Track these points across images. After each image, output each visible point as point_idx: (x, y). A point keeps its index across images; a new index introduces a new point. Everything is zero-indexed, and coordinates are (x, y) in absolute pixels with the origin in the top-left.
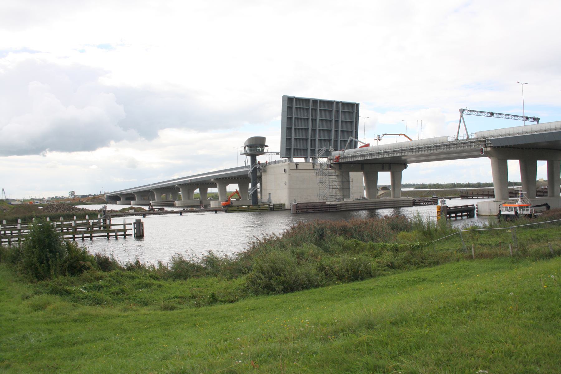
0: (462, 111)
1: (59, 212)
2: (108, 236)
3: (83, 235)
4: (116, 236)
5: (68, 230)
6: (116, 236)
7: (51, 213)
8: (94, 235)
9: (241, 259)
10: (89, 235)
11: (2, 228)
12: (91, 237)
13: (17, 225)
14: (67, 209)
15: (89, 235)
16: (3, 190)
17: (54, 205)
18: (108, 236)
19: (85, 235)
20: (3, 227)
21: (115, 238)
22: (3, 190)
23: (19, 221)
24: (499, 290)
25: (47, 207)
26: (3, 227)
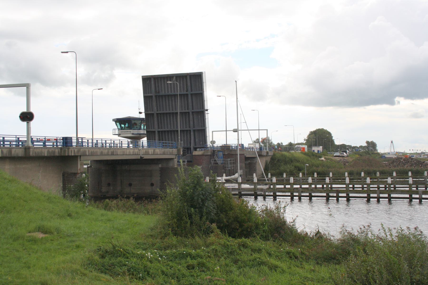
0: (267, 130)
1: (405, 167)
2: (411, 199)
3: (378, 195)
4: (338, 197)
5: (417, 189)
6: (338, 197)
7: (397, 168)
8: (392, 195)
9: (289, 228)
10: (386, 195)
11: (391, 181)
12: (311, 197)
13: (409, 179)
14: (415, 164)
15: (386, 195)
16: (392, 142)
17: (401, 158)
18: (411, 199)
19: (381, 195)
20: (392, 180)
21: (325, 201)
22: (392, 142)
23: (410, 174)
24: (159, 248)
25: (393, 161)
26: (392, 180)
